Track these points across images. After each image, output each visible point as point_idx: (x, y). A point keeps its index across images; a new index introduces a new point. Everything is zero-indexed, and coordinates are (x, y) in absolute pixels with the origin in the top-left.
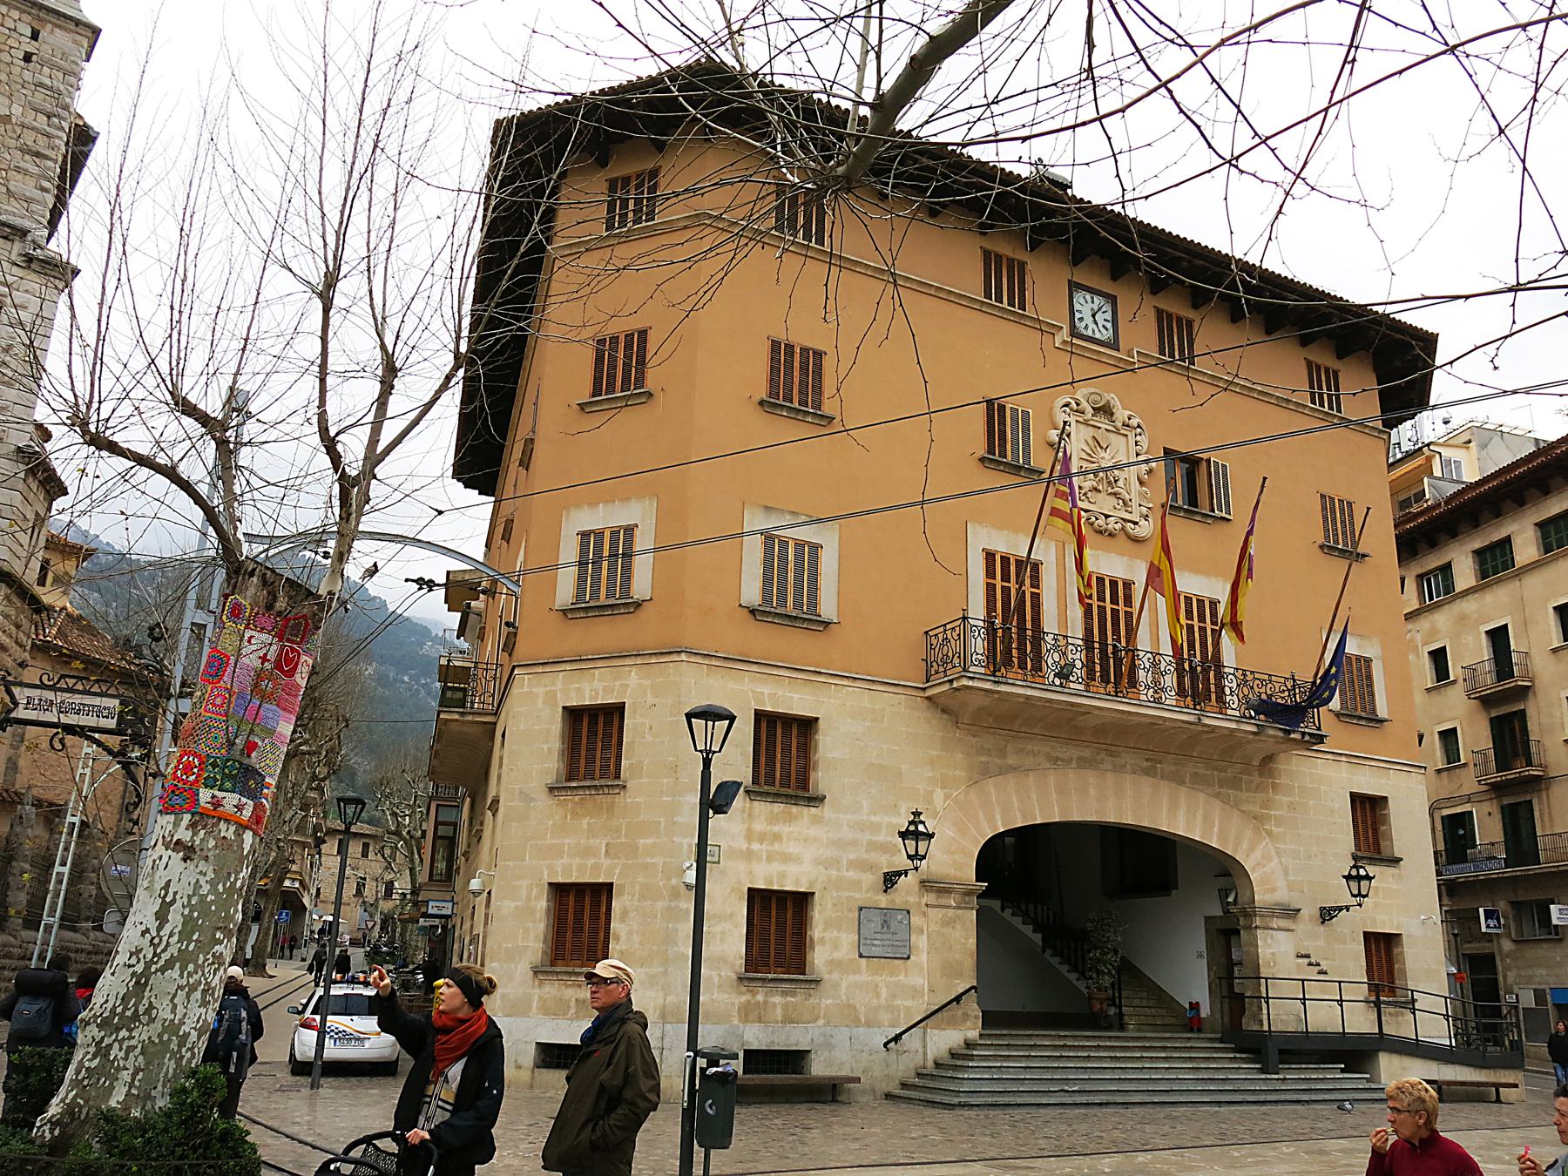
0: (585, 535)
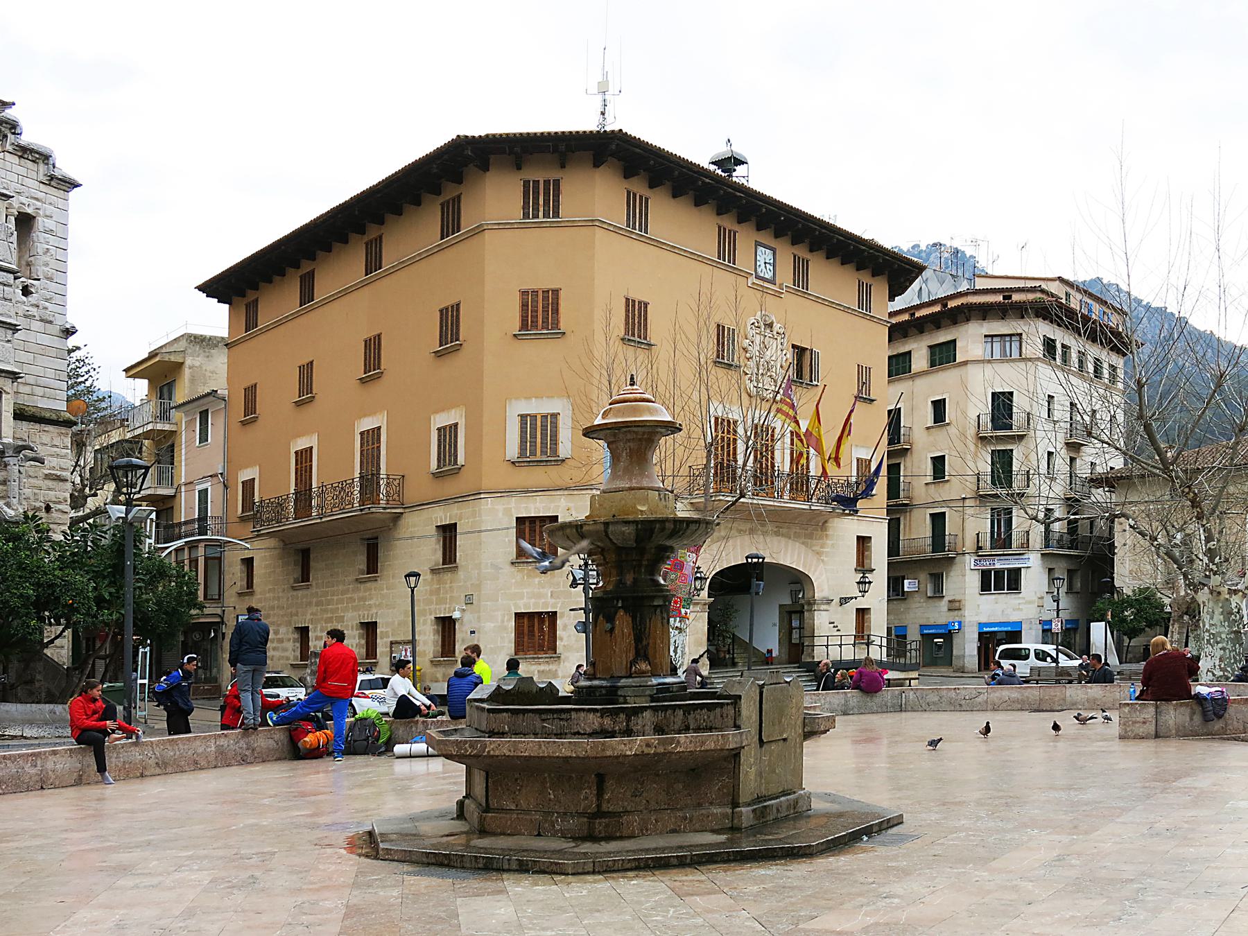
0: (523, 417)
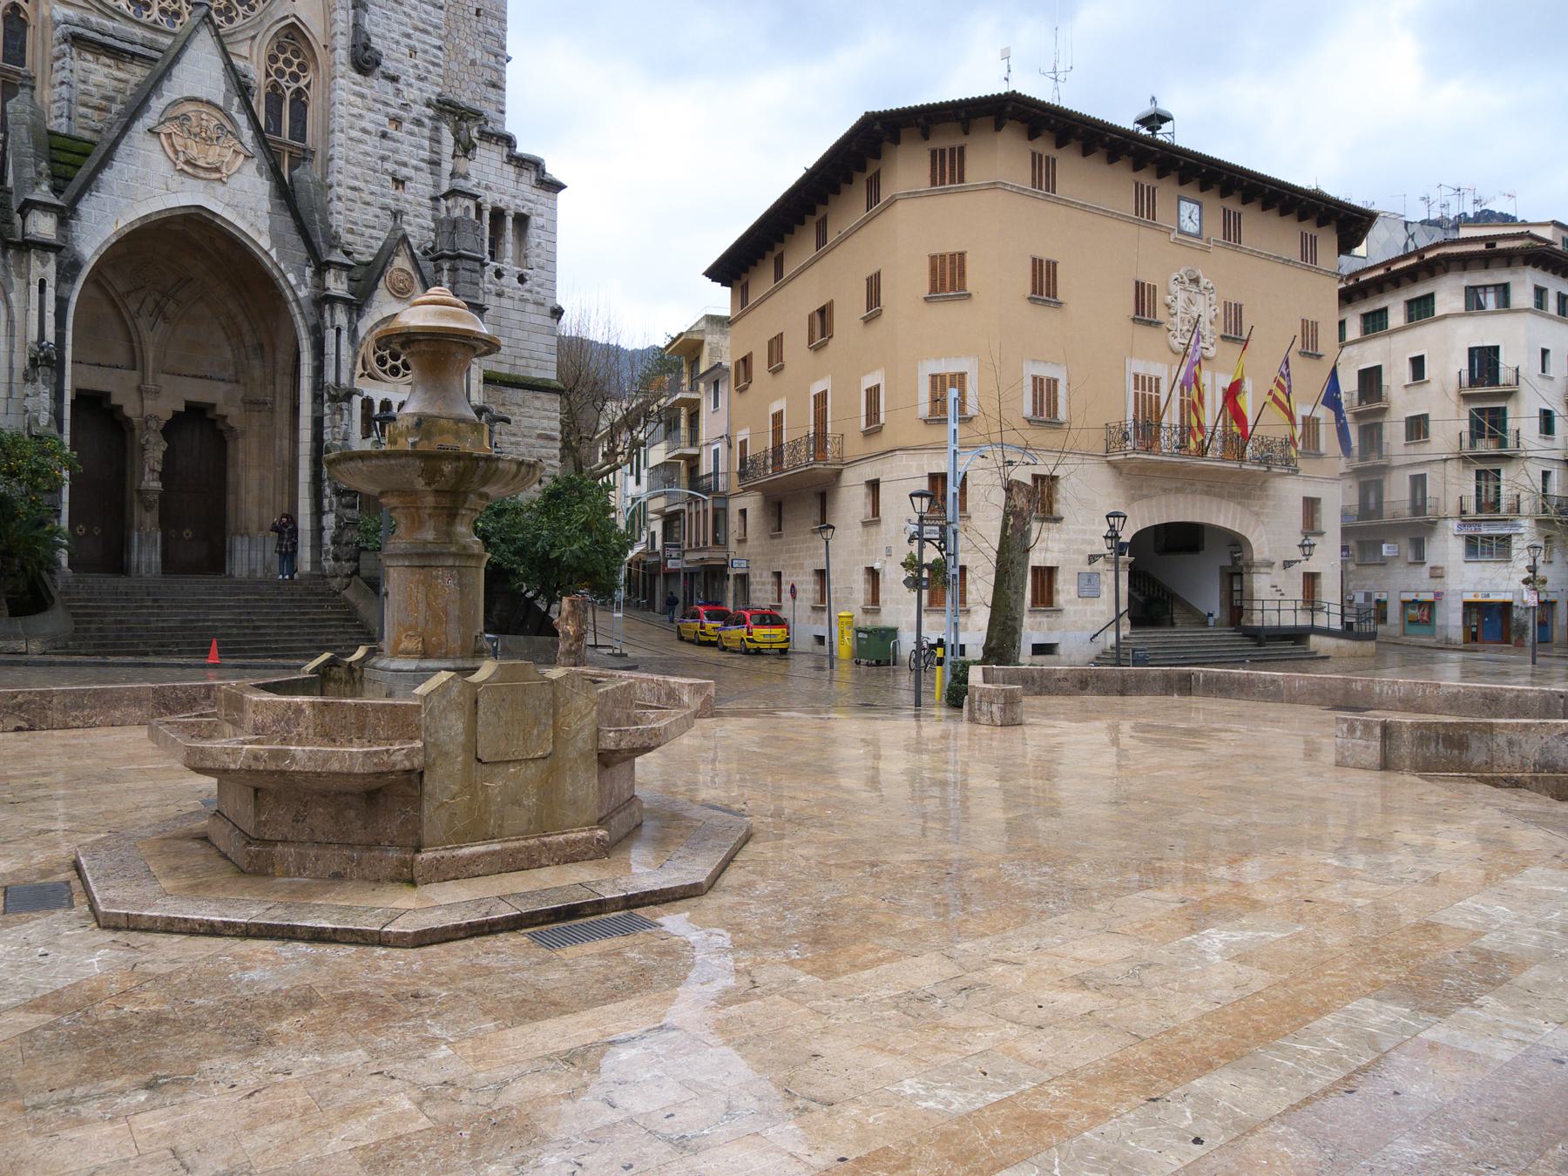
0: (934, 377)
